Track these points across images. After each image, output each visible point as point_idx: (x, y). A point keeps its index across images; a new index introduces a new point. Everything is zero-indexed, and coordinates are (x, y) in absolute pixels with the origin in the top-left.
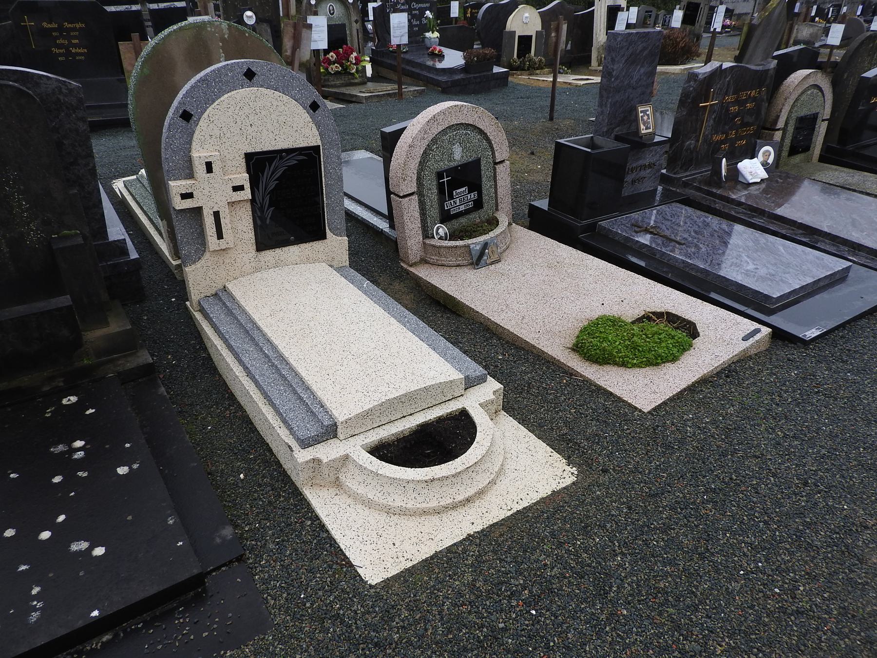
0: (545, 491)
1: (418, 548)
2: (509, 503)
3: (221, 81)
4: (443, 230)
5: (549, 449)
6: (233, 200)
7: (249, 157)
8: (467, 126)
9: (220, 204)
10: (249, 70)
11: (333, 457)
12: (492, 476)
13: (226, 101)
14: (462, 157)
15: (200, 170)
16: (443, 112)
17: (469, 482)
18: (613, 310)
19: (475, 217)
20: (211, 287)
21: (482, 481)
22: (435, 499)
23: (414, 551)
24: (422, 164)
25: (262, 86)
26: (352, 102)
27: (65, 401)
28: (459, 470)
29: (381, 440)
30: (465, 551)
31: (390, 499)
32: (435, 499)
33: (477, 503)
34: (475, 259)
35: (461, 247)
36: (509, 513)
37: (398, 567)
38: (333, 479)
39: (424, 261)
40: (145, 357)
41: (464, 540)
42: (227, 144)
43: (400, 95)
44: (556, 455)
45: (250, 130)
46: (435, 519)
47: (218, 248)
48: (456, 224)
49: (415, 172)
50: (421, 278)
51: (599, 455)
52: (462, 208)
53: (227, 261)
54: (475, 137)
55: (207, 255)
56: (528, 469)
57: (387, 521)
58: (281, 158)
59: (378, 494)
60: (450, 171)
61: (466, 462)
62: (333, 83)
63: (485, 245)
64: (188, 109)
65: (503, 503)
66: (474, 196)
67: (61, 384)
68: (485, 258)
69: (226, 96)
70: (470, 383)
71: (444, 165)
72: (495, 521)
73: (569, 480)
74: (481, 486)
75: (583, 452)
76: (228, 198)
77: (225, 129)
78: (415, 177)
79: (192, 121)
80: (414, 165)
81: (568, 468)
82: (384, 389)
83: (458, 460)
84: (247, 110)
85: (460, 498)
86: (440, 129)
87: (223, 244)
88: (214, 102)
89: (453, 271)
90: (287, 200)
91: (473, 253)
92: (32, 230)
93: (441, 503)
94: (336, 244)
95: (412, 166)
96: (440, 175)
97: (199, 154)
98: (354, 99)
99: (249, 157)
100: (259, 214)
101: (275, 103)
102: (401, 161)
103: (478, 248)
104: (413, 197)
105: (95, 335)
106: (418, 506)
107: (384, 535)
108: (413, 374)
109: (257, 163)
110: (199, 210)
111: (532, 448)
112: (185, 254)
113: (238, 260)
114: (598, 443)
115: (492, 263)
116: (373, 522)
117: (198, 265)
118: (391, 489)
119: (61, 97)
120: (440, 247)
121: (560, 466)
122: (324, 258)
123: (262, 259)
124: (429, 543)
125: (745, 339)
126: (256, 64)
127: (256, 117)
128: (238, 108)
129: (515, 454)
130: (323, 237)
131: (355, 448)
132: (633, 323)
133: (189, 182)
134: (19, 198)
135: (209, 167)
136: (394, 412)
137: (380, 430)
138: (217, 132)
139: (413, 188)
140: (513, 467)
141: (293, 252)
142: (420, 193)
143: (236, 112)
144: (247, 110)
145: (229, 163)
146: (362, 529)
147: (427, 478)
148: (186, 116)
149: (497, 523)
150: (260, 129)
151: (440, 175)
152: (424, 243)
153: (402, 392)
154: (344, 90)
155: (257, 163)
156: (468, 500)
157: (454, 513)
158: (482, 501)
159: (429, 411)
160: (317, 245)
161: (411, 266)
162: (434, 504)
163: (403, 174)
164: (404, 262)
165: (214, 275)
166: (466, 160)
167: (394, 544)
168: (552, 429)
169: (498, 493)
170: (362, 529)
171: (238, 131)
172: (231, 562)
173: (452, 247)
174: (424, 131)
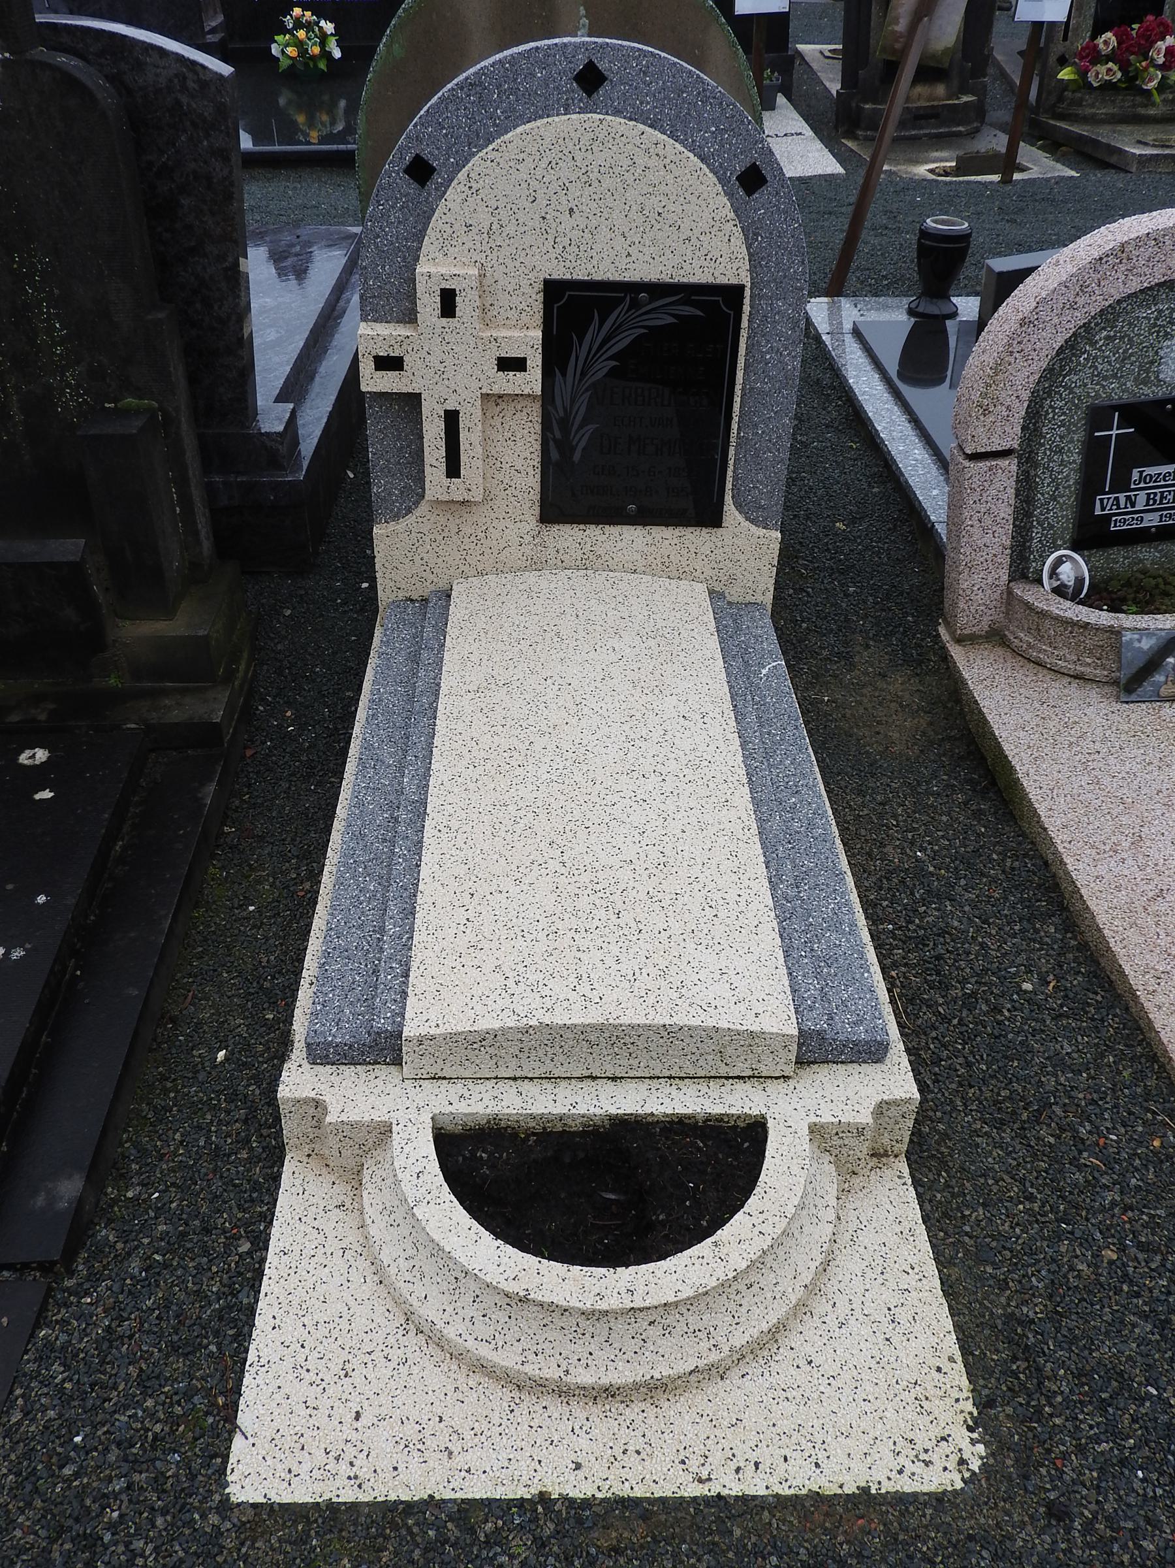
0: (841, 1474)
1: (400, 1458)
2: (716, 1458)
3: (513, 91)
5: (951, 1345)
6: (496, 390)
7: (553, 290)
9: (465, 394)
10: (590, 66)
11: (353, 1116)
12: (714, 1357)
13: (517, 142)
15: (428, 305)
16: (1155, 239)
17: (632, 1345)
20: (423, 580)
21: (672, 1357)
22: (518, 1347)
23: (385, 1464)
24: (1051, 375)
25: (617, 112)
26: (1105, 165)
27: (24, 758)
28: (603, 1306)
29: (496, 1118)
30: (496, 1540)
31: (420, 1291)
32: (518, 1347)
33: (632, 1413)
34: (1124, 676)
35: (1098, 629)
36: (693, 1490)
37: (318, 1487)
38: (351, 1163)
39: (996, 637)
40: (214, 707)
41: (521, 1503)
42: (506, 251)
44: (958, 1376)
45: (567, 222)
46: (500, 1397)
47: (446, 498)
48: (1120, 559)
49: (1026, 395)
50: (964, 682)
51: (1081, 1450)
52: (1152, 520)
53: (467, 530)
55: (423, 508)
56: (846, 1376)
57: (391, 1340)
58: (635, 304)
59: (401, 1261)
60: (1131, 412)
61: (641, 1290)
62: (1089, 111)
64: (425, 155)
65: (700, 1449)
67: (43, 717)
68: (1159, 678)
69: (519, 130)
70: (815, 1050)
71: (1117, 391)
72: (639, 1492)
73: (939, 1478)
74: (662, 1370)
75: (1039, 1411)
76: (483, 383)
77: (504, 214)
78: (1020, 410)
79: (431, 185)
80: (1024, 377)
81: (962, 1437)
82: (559, 988)
83: (625, 1275)
84: (565, 171)
85: (585, 1377)
86: (1134, 285)
87: (457, 489)
88: (489, 142)
89: (1057, 688)
90: (638, 409)
91: (1127, 655)
92: (69, 385)
93: (528, 1368)
94: (747, 548)
96: (1098, 416)
97: (434, 267)
98: (1113, 160)
99: (553, 290)
100: (558, 435)
101: (641, 161)
102: (989, 359)
103: (1146, 644)
104: (1003, 463)
105: (139, 632)
106: (471, 1344)
107: (357, 1378)
108: (664, 973)
109: (571, 307)
110: (413, 401)
111: (903, 1315)
112: (378, 495)
113: (495, 534)
114: (1103, 1406)
116: (360, 1323)
117: (401, 525)
118: (429, 1268)
119: (184, 100)
120: (1043, 614)
121: (944, 1418)
122: (709, 572)
123: (551, 543)
124: (434, 1458)
126: (617, 51)
127: (588, 190)
128: (545, 161)
129: (843, 1309)
130: (712, 518)
131: (407, 1111)
133: (402, 331)
134: (48, 313)
135: (448, 303)
136: (562, 1058)
137: (510, 1089)
138: (483, 218)
139: (1010, 437)
140: (809, 1349)
141: (630, 540)
142: (1027, 454)
143: (539, 172)
144: (565, 171)
145: (504, 299)
146: (323, 1330)
147: (512, 1287)
148: (420, 171)
149: (636, 1502)
150: (594, 223)
152: (1010, 592)
153: (593, 1017)
154: (1104, 134)
155: (571, 307)
156: (610, 1392)
157: (557, 1408)
158: (651, 1411)
159: (666, 1088)
160: (696, 538)
161: (959, 641)
162: (507, 1359)
163: (984, 395)
164: (947, 624)
165: (432, 554)
167: (358, 1416)
168: (1003, 1285)
169: (709, 1409)
170: (323, 1330)
171: (537, 222)
172: (26, 1266)
173: (1074, 624)
174: (1080, 284)
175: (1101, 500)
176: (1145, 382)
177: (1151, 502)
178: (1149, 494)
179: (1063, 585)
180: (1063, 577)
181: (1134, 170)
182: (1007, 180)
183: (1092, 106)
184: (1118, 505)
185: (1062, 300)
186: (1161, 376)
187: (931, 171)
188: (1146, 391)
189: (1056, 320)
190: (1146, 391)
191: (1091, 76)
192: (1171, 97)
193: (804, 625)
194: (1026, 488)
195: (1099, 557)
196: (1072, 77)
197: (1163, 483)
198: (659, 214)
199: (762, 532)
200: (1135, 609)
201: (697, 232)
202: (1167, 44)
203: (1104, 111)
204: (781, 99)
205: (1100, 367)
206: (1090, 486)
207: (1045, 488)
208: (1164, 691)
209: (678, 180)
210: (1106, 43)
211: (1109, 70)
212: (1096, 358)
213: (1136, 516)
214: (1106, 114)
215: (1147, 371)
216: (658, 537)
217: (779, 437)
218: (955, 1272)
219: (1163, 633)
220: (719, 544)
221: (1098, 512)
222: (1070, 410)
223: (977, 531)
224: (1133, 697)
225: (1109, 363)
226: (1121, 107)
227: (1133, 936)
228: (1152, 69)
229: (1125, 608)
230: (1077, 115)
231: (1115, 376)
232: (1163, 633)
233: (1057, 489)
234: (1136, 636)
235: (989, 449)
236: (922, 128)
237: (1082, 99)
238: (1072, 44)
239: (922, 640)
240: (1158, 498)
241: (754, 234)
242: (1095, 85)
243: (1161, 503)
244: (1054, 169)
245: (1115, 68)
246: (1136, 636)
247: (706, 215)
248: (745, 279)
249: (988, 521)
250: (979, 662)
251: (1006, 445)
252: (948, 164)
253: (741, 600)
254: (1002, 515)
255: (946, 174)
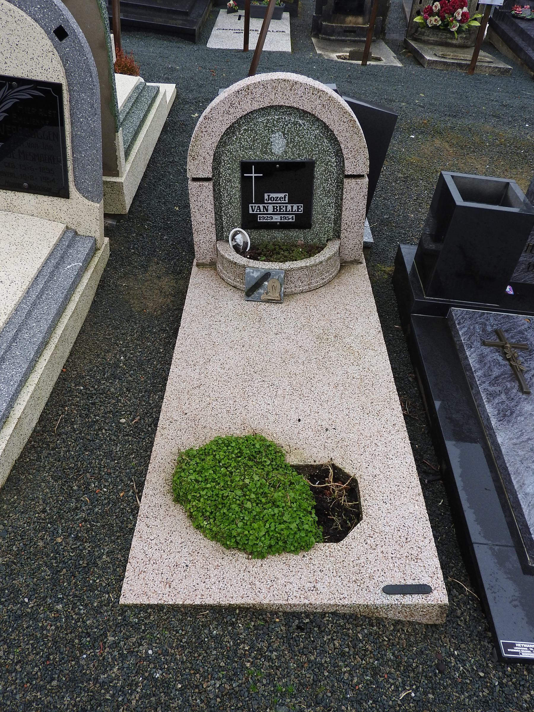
4: (243, 237)
8: (304, 114)
14: (286, 152)
18: (276, 432)
19: (299, 236)
24: (222, 143)
43: (471, 67)
48: (266, 236)
49: (212, 153)
52: (277, 219)
54: (312, 133)
60: (261, 166)
62: (426, 38)
63: (266, 276)
66: (297, 208)
68: (261, 291)
71: (254, 155)
86: (256, 106)
95: (208, 144)
96: (245, 167)
103: (256, 275)
104: (206, 184)
115: (268, 301)
122: (68, 220)
125: (390, 590)
130: (65, 194)
132: (299, 469)
151: (245, 167)
166: (290, 157)
175: (252, 207)
176: (266, 153)
177: (275, 210)
178: (274, 206)
179: (238, 244)
180: (238, 241)
181: (426, 67)
182: (364, 64)
183: (428, 36)
184: (260, 209)
185: (223, 109)
186: (273, 151)
187: (339, 57)
188: (266, 157)
189: (221, 119)
190: (266, 157)
191: (428, 21)
192: (464, 36)
193: (133, 251)
194: (217, 196)
195: (256, 234)
196: (420, 21)
197: (279, 202)
198: (17, 45)
199: (90, 203)
200: (263, 259)
201: (36, 56)
202: (463, 11)
203: (432, 39)
204: (286, 15)
205: (243, 143)
206: (246, 200)
207: (225, 199)
208: (263, 297)
209: (23, 29)
210: (436, 7)
211: (436, 20)
212: (240, 138)
213: (269, 216)
214: (434, 40)
215: (266, 148)
216: (41, 200)
217: (93, 159)
218: (444, 570)
219: (263, 270)
220: (71, 207)
221: (251, 212)
222: (232, 162)
223: (198, 216)
224: (250, 299)
225: (247, 141)
226: (440, 38)
227: (175, 403)
228: (454, 22)
229: (259, 258)
230: (421, 39)
231: (251, 148)
232: (263, 270)
233: (231, 199)
234: (252, 271)
235: (198, 176)
236: (347, 37)
237: (424, 32)
238: (424, 6)
239: (185, 263)
240: (278, 208)
241: (66, 60)
242: (430, 26)
243: (280, 211)
244: (392, 62)
245: (439, 19)
246: (252, 271)
247: (39, 47)
248: (63, 81)
249: (202, 211)
250: (200, 276)
251: (206, 176)
252: (346, 54)
253: (84, 234)
254: (209, 209)
255: (345, 59)
